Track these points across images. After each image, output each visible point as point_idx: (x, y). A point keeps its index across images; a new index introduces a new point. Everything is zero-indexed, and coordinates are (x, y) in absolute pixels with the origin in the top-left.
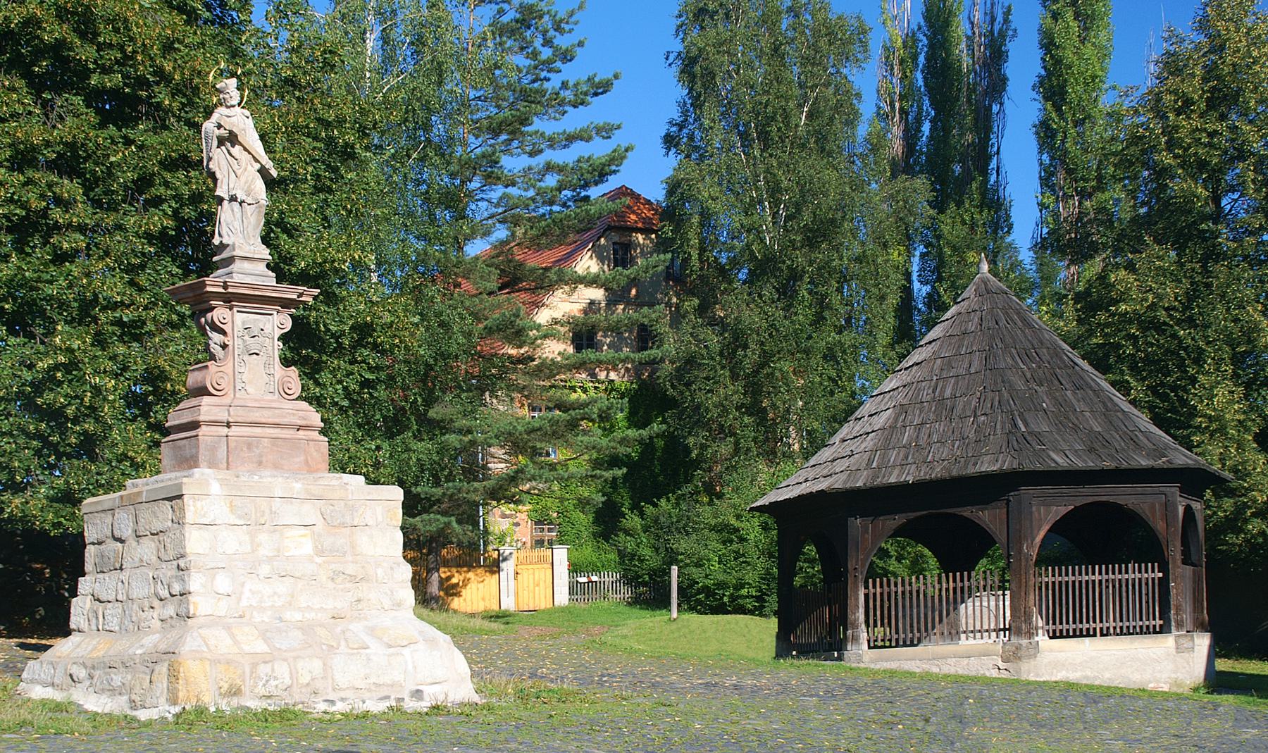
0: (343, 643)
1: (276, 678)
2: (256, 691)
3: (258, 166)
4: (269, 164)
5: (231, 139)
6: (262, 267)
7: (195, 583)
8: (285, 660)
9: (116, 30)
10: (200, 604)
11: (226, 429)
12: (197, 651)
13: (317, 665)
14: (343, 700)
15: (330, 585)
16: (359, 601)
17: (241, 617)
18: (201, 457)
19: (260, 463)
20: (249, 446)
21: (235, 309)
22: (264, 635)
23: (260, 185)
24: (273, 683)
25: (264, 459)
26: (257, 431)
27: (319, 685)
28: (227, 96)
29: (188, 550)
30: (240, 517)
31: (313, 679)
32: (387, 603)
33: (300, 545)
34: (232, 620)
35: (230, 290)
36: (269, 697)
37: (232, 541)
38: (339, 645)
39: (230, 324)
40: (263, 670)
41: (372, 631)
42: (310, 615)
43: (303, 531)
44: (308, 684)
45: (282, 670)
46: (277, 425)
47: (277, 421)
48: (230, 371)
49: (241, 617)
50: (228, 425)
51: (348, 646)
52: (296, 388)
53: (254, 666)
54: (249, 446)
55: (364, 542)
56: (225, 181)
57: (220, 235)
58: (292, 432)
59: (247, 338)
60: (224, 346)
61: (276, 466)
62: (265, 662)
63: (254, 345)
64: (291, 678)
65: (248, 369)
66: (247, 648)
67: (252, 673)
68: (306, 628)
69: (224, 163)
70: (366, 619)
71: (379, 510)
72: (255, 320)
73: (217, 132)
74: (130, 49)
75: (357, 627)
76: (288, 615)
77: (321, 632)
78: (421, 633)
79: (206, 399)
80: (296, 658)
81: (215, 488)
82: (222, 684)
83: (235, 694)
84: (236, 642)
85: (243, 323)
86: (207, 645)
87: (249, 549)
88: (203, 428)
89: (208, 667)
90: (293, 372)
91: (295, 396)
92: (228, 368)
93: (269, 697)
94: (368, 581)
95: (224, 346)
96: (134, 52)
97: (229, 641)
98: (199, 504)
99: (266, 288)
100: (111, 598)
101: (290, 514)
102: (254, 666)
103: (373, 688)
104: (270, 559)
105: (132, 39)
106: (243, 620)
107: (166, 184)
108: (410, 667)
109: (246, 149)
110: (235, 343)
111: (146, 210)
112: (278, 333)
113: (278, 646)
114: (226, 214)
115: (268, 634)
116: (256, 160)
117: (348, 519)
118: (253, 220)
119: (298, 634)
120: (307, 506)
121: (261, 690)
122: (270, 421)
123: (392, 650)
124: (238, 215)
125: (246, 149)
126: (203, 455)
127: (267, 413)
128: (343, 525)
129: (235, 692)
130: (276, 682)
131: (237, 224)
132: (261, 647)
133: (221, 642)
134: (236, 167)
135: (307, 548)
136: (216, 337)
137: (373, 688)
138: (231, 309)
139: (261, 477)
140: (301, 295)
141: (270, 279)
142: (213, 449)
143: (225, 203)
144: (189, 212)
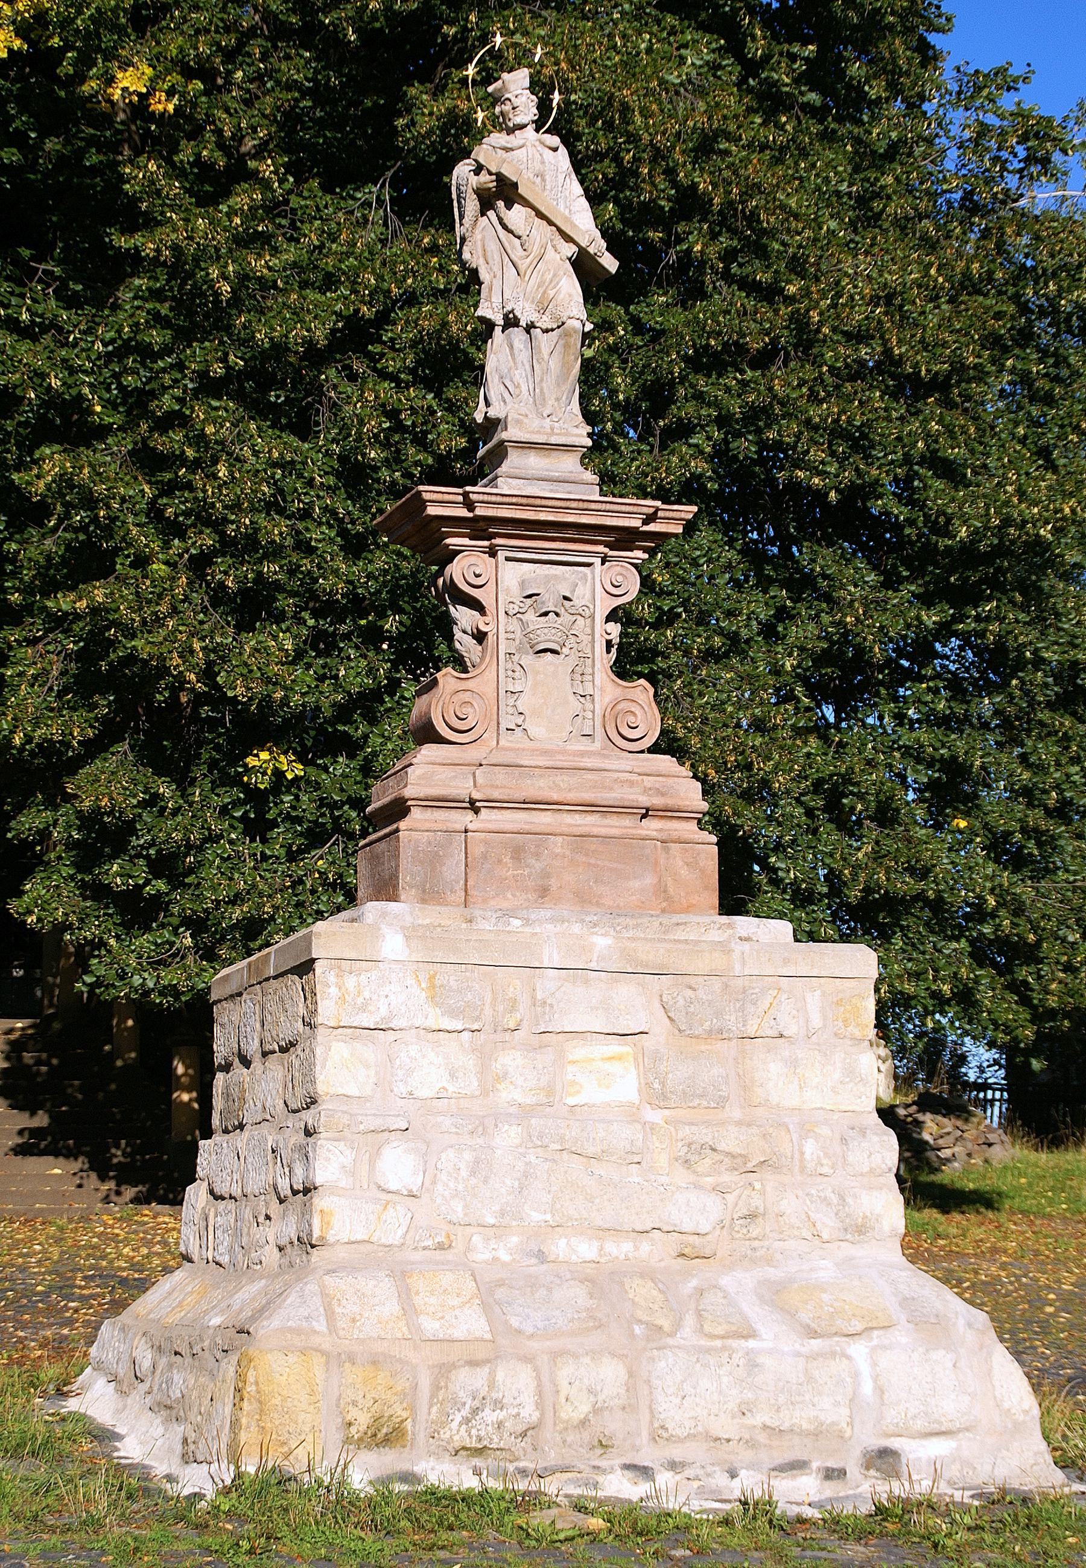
0: (690, 1320)
1: (499, 1405)
2: (445, 1435)
3: (571, 250)
4: (598, 246)
5: (503, 192)
6: (570, 464)
7: (329, 1165)
8: (527, 1359)
9: (609, 126)
10: (339, 1217)
11: (470, 815)
12: (297, 1331)
13: (610, 1375)
14: (673, 1466)
15: (681, 1176)
16: (752, 1216)
17: (440, 1247)
18: (404, 879)
19: (544, 892)
20: (518, 854)
21: (501, 555)
22: (489, 1295)
23: (570, 289)
24: (490, 1416)
25: (554, 883)
26: (543, 819)
27: (613, 1425)
28: (507, 107)
29: (321, 1088)
30: (453, 1013)
31: (597, 1411)
32: (827, 1224)
33: (607, 1081)
34: (418, 1256)
35: (479, 512)
36: (480, 1452)
37: (431, 1070)
38: (678, 1325)
39: (491, 585)
40: (468, 1382)
41: (775, 1295)
42: (620, 1249)
43: (616, 1047)
44: (584, 1423)
45: (517, 1385)
46: (590, 807)
47: (588, 796)
48: (490, 691)
49: (440, 1247)
50: (473, 806)
51: (700, 1330)
52: (648, 722)
53: (444, 1371)
54: (518, 854)
55: (777, 1081)
56: (497, 289)
57: (488, 404)
58: (627, 821)
59: (530, 616)
60: (480, 637)
61: (584, 899)
62: (473, 1363)
63: (546, 632)
64: (539, 1405)
65: (542, 681)
66: (430, 1326)
67: (436, 1388)
68: (601, 1281)
69: (493, 247)
70: (769, 1261)
71: (814, 1001)
72: (548, 579)
73: (474, 180)
74: (628, 157)
75: (739, 1284)
76: (559, 1247)
77: (641, 1291)
78: (906, 1302)
79: (429, 751)
80: (556, 1355)
81: (393, 945)
82: (353, 1414)
83: (387, 1441)
84: (409, 1309)
85: (523, 584)
86: (330, 1316)
87: (473, 1085)
88: (416, 814)
89: (319, 1372)
90: (642, 691)
91: (648, 742)
92: (483, 681)
93: (480, 1452)
94: (777, 1169)
95: (480, 637)
96: (636, 160)
97: (392, 1308)
98: (351, 982)
99: (584, 506)
100: (237, 1191)
101: (579, 1008)
102: (444, 1371)
103: (762, 1438)
104: (524, 1113)
105: (633, 139)
106: (449, 1255)
107: (699, 397)
108: (867, 1388)
109: (540, 215)
110: (501, 628)
111: (663, 447)
112: (604, 606)
113: (515, 1322)
114: (501, 356)
115: (501, 1293)
116: (568, 239)
117: (731, 1021)
118: (554, 364)
119: (579, 1294)
120: (627, 991)
121: (457, 1434)
122: (572, 797)
123: (816, 1344)
124: (524, 356)
125: (540, 215)
126: (408, 872)
127: (564, 780)
128: (719, 1034)
129: (385, 1435)
130: (499, 1415)
131: (520, 375)
132: (471, 1323)
133: (369, 1307)
134: (517, 253)
135: (626, 1086)
136: (463, 615)
137: (762, 1438)
138: (492, 553)
139: (527, 922)
140: (650, 519)
141: (584, 485)
142: (433, 860)
143: (498, 330)
144: (745, 446)
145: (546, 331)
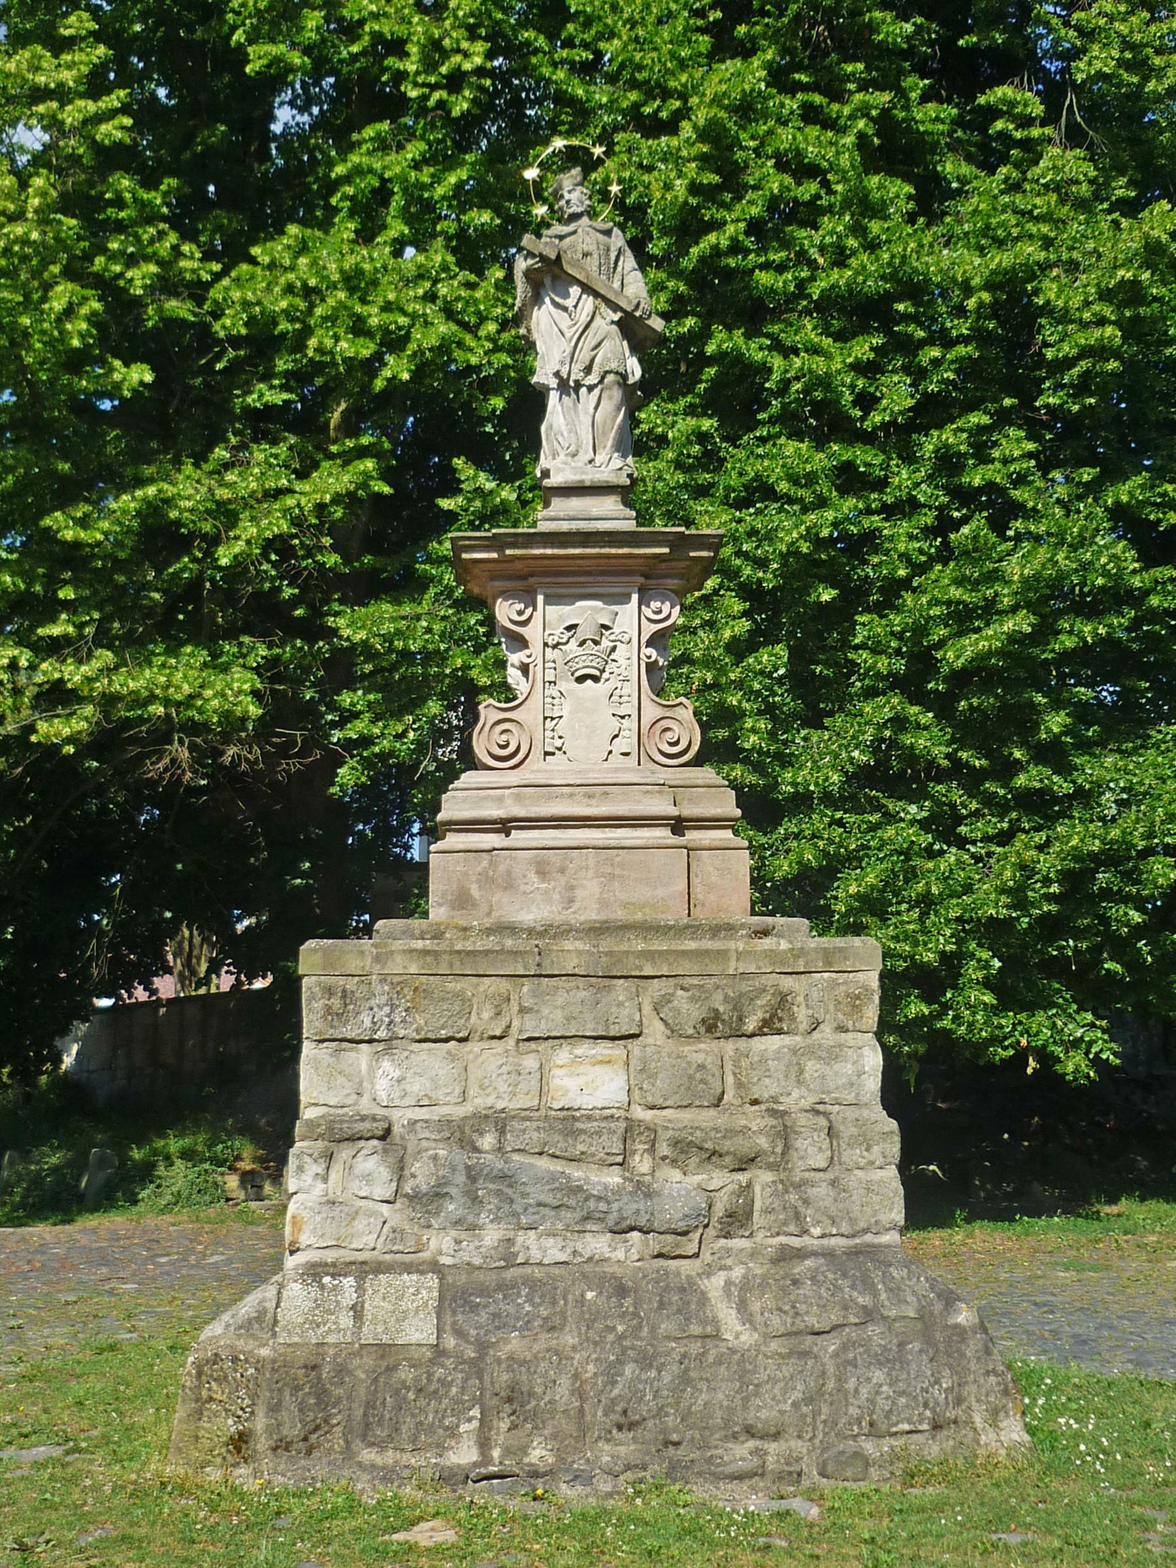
43: (603, 1049)
145: (590, 389)
